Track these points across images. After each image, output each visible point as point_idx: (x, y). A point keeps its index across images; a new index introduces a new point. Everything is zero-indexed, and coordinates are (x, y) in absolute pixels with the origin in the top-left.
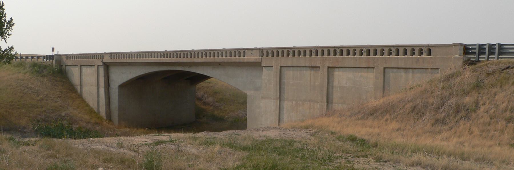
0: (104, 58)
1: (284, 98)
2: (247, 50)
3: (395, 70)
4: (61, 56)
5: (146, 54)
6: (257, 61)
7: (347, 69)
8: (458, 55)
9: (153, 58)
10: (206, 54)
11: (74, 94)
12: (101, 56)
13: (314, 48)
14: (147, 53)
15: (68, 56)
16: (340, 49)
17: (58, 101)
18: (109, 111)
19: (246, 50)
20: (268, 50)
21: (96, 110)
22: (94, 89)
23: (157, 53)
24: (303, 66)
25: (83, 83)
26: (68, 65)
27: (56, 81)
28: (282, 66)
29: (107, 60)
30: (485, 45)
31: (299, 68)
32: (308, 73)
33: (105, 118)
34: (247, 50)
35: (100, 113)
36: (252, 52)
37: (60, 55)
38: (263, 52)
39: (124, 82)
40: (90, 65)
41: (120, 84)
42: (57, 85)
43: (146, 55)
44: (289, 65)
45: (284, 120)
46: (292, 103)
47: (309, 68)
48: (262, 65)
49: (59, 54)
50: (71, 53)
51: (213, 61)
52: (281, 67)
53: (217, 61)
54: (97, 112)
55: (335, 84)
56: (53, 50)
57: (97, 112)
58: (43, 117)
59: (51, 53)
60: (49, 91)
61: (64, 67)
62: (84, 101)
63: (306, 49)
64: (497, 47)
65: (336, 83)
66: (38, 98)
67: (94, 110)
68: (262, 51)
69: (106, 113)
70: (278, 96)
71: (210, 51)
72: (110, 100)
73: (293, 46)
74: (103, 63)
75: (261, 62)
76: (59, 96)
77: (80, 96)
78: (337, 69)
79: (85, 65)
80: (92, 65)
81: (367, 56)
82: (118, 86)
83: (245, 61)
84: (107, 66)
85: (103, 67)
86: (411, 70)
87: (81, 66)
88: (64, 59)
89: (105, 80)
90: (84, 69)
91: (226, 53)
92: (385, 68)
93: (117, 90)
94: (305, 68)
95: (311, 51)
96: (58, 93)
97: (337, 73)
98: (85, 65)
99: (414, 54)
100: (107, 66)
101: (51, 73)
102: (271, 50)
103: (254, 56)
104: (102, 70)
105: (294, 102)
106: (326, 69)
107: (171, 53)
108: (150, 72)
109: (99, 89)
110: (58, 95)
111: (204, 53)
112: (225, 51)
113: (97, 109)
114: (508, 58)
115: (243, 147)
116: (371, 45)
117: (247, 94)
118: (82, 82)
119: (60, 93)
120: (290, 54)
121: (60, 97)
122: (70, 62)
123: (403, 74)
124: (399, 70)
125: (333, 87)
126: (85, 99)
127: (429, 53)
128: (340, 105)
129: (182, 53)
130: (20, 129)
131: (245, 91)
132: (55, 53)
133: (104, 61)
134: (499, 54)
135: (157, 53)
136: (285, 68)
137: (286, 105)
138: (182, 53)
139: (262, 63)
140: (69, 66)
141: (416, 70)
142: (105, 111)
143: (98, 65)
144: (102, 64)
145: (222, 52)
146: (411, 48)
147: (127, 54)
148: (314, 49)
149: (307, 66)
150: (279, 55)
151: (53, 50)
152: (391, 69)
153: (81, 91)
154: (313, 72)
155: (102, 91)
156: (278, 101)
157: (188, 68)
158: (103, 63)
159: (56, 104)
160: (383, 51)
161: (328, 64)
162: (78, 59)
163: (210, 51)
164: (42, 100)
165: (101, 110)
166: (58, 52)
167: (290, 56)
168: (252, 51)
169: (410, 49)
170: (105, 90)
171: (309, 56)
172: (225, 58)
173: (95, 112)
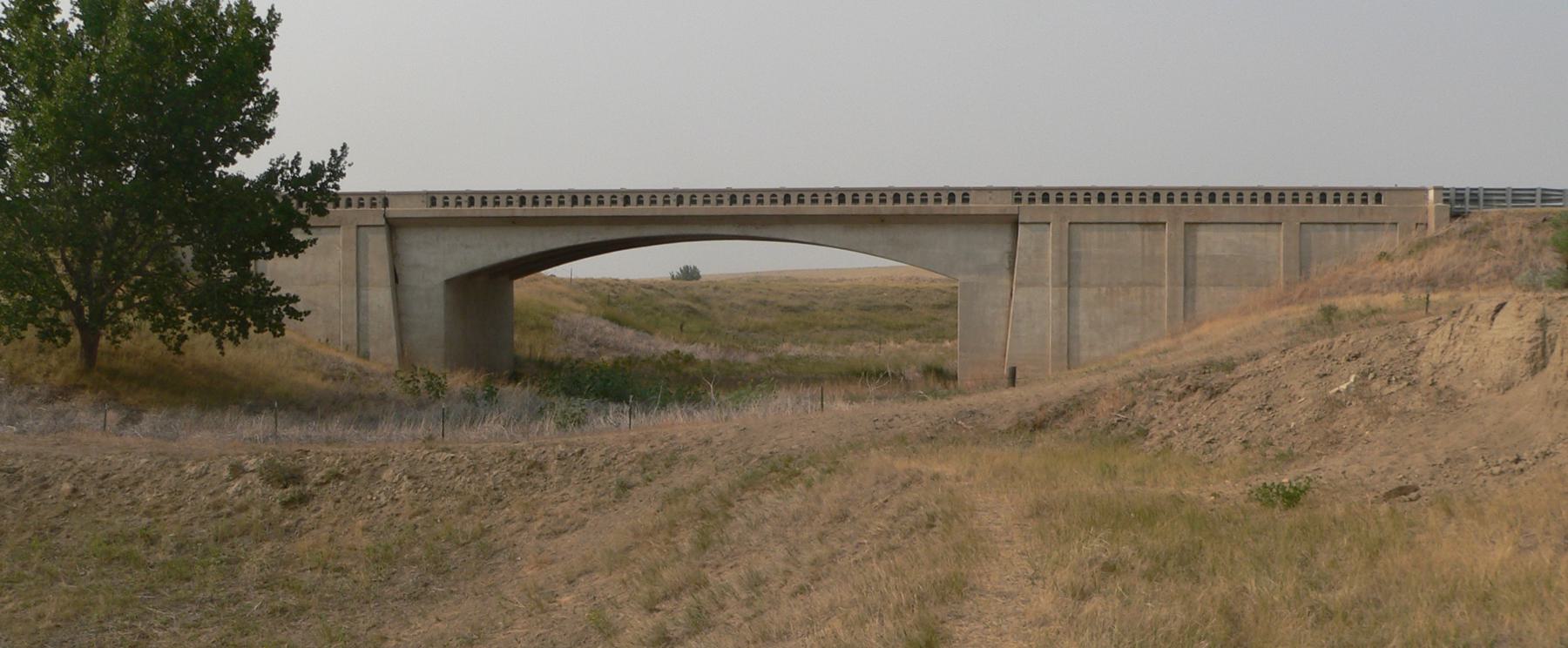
3: (1319, 227)
7: (1248, 226)
8: (1010, 196)
12: (385, 199)
28: (360, 224)
29: (395, 210)
31: (1114, 226)
32: (1136, 235)
41: (449, 277)
46: (1100, 290)
55: (1198, 252)
65: (1201, 250)
78: (1202, 227)
86: (1347, 226)
92: (1301, 223)
93: (439, 293)
97: (1203, 233)
98: (1081, 223)
104: (378, 242)
106: (1181, 227)
114: (1526, 206)
115: (867, 401)
123: (1333, 231)
124: (1325, 227)
125: (1194, 257)
127: (1378, 199)
128: (1212, 288)
130: (276, 404)
133: (390, 215)
134: (1543, 201)
141: (1357, 226)
143: (359, 227)
144: (383, 222)
152: (1311, 226)
161: (1185, 218)
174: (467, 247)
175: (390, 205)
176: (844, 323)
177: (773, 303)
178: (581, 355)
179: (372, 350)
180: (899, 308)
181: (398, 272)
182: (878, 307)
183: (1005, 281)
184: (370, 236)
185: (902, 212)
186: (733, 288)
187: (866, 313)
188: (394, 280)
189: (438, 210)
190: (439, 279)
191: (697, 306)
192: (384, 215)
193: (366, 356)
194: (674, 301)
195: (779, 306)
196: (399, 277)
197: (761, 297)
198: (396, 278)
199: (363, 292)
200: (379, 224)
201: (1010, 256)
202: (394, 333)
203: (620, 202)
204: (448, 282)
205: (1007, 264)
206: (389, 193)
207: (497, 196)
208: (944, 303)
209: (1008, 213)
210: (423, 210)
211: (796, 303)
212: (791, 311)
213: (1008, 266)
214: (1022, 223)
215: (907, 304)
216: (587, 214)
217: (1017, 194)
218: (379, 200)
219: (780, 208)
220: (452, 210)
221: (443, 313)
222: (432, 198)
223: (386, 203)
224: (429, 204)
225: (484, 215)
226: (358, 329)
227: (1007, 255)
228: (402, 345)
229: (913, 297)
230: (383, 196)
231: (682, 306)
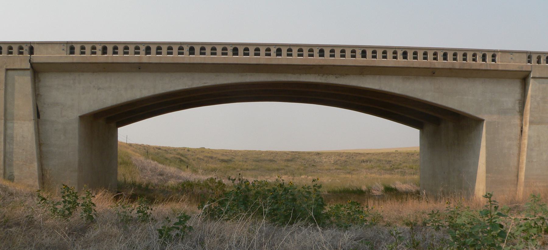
0: (35, 52)
8: (525, 57)
12: (31, 48)
28: (8, 68)
29: (39, 56)
36: (512, 56)
51: (429, 67)
93: (74, 128)
133: (35, 61)
143: (7, 70)
144: (29, 66)
157: (336, 78)
168: (512, 54)
174: (99, 89)
175: (35, 53)
176: (249, 167)
177: (215, 158)
178: (156, 181)
179: (16, 173)
180: (271, 161)
181: (39, 109)
182: (262, 160)
183: (516, 121)
184: (16, 78)
185: (451, 67)
186: (196, 151)
187: (258, 163)
188: (36, 116)
189: (77, 57)
190: (74, 115)
191: (183, 158)
192: (30, 60)
193: (11, 179)
194: (172, 156)
195: (219, 159)
196: (41, 113)
197: (209, 155)
198: (38, 114)
199: (9, 125)
200: (25, 68)
201: (519, 103)
202: (36, 159)
203: (230, 52)
204: (83, 118)
205: (517, 108)
206: (34, 43)
207: (126, 47)
208: (290, 159)
209: (524, 70)
210: (64, 57)
211: (225, 158)
212: (224, 161)
213: (518, 111)
214: (533, 78)
215: (274, 159)
216: (203, 62)
217: (529, 56)
218: (26, 48)
219: (359, 61)
220: (88, 57)
221: (77, 142)
222: (71, 47)
223: (31, 51)
224: (68, 52)
225: (115, 61)
226: (5, 156)
227: (517, 102)
228: (39, 134)
229: (275, 156)
230: (29, 45)
231: (177, 158)
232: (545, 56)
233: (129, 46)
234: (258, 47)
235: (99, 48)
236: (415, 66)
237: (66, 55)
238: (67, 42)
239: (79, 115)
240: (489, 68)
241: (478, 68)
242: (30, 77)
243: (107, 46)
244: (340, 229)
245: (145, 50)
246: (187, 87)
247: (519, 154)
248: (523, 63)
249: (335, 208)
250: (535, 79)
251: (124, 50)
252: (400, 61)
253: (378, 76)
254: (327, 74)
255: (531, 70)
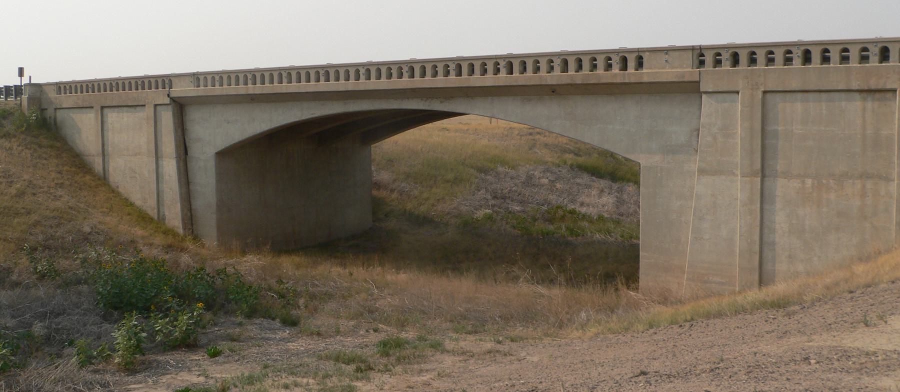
0: (174, 85)
1: (776, 170)
2: (648, 51)
4: (41, 87)
5: (76, 86)
6: (686, 80)
8: (689, 56)
9: (294, 84)
10: (327, 74)
11: (88, 177)
12: (165, 81)
13: (452, 60)
14: (108, 81)
15: (61, 87)
16: (409, 66)
17: (61, 196)
18: (189, 214)
19: (648, 53)
20: (319, 70)
21: (153, 214)
22: (146, 165)
23: (81, 84)
24: (840, 88)
25: (109, 149)
26: (64, 107)
27: (40, 146)
28: (156, 103)
29: (180, 90)
30: (12, 87)
32: (854, 106)
33: (181, 231)
34: (648, 51)
35: (164, 219)
36: (667, 56)
37: (39, 86)
38: (198, 79)
39: (233, 142)
40: (130, 104)
41: (220, 149)
42: (44, 155)
43: (150, 82)
44: (794, 86)
45: (777, 226)
46: (803, 182)
47: (857, 95)
48: (702, 90)
49: (32, 82)
50: (92, 78)
51: (538, 83)
52: (765, 92)
53: (549, 83)
54: (156, 217)
56: (21, 72)
57: (156, 217)
58: (41, 237)
59: (14, 81)
60: (31, 170)
61: (50, 113)
62: (114, 192)
63: (348, 68)
64: (13, 88)
66: (13, 191)
67: (148, 214)
68: (699, 54)
69: (183, 220)
70: (758, 166)
71: (130, 80)
72: (192, 187)
73: (365, 61)
74: (171, 98)
75: (698, 82)
76: (57, 184)
77: (103, 180)
79: (86, 108)
80: (136, 104)
81: (456, 76)
82: (214, 152)
83: (646, 79)
84: (180, 106)
85: (170, 107)
87: (102, 108)
88: (52, 94)
89: (176, 141)
90: (112, 117)
91: (229, 78)
93: (212, 164)
94: (843, 95)
95: (318, 73)
96: (53, 175)
99: (526, 71)
100: (180, 106)
101: (24, 129)
102: (220, 75)
103: (673, 68)
104: (167, 118)
105: (809, 182)
107: (151, 80)
108: (314, 116)
109: (160, 162)
110: (56, 181)
111: (90, 86)
112: (227, 75)
113: (156, 211)
116: (465, 56)
117: (639, 164)
118: (106, 147)
119: (59, 176)
120: (284, 78)
121: (61, 185)
122: (67, 100)
126: (118, 187)
129: (127, 83)
131: (631, 157)
132: (25, 80)
133: (172, 95)
135: (81, 84)
136: (778, 97)
137: (782, 188)
138: (127, 83)
139: (701, 83)
140: (66, 110)
142: (180, 215)
143: (156, 106)
144: (167, 101)
145: (143, 81)
146: (605, 56)
147: (150, 81)
148: (407, 66)
149: (853, 88)
150: (381, 77)
151: (21, 72)
153: (104, 168)
154: (869, 105)
155: (170, 167)
156: (759, 179)
157: (441, 102)
158: (171, 98)
159: (58, 204)
160: (485, 67)
162: (93, 92)
163: (124, 79)
164: (21, 194)
165: (166, 213)
166: (30, 77)
167: (893, 62)
168: (667, 54)
169: (443, 66)
170: (178, 163)
171: (345, 81)
172: (518, 75)
173: (152, 219)
232: (727, 52)
233: (539, 59)
234: (594, 56)
235: (874, 51)
236: (520, 84)
237: (194, 87)
238: (693, 46)
239: (217, 150)
240: (627, 81)
241: (610, 81)
242: (171, 113)
243: (890, 46)
244: (105, 212)
245: (878, 54)
246: (297, 120)
247: (740, 226)
248: (686, 68)
249: (577, 298)
250: (708, 95)
251: (841, 54)
252: (503, 78)
253: (490, 98)
254: (436, 98)
255: (698, 80)
